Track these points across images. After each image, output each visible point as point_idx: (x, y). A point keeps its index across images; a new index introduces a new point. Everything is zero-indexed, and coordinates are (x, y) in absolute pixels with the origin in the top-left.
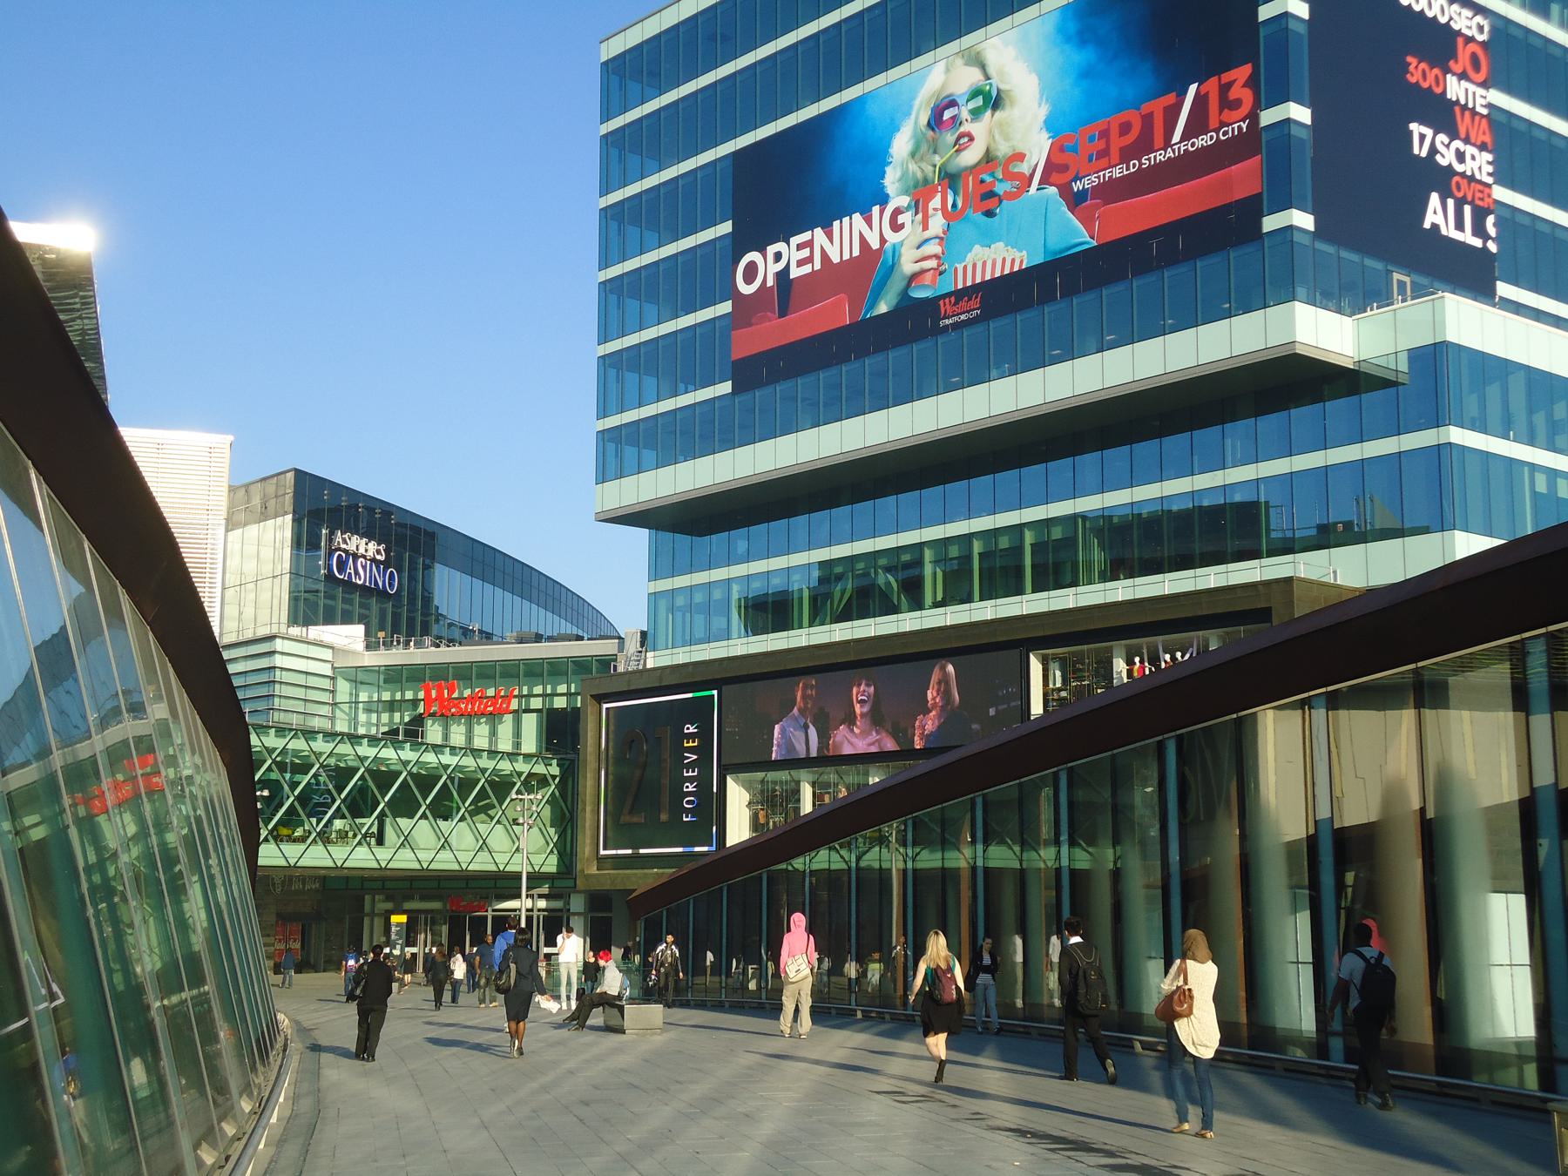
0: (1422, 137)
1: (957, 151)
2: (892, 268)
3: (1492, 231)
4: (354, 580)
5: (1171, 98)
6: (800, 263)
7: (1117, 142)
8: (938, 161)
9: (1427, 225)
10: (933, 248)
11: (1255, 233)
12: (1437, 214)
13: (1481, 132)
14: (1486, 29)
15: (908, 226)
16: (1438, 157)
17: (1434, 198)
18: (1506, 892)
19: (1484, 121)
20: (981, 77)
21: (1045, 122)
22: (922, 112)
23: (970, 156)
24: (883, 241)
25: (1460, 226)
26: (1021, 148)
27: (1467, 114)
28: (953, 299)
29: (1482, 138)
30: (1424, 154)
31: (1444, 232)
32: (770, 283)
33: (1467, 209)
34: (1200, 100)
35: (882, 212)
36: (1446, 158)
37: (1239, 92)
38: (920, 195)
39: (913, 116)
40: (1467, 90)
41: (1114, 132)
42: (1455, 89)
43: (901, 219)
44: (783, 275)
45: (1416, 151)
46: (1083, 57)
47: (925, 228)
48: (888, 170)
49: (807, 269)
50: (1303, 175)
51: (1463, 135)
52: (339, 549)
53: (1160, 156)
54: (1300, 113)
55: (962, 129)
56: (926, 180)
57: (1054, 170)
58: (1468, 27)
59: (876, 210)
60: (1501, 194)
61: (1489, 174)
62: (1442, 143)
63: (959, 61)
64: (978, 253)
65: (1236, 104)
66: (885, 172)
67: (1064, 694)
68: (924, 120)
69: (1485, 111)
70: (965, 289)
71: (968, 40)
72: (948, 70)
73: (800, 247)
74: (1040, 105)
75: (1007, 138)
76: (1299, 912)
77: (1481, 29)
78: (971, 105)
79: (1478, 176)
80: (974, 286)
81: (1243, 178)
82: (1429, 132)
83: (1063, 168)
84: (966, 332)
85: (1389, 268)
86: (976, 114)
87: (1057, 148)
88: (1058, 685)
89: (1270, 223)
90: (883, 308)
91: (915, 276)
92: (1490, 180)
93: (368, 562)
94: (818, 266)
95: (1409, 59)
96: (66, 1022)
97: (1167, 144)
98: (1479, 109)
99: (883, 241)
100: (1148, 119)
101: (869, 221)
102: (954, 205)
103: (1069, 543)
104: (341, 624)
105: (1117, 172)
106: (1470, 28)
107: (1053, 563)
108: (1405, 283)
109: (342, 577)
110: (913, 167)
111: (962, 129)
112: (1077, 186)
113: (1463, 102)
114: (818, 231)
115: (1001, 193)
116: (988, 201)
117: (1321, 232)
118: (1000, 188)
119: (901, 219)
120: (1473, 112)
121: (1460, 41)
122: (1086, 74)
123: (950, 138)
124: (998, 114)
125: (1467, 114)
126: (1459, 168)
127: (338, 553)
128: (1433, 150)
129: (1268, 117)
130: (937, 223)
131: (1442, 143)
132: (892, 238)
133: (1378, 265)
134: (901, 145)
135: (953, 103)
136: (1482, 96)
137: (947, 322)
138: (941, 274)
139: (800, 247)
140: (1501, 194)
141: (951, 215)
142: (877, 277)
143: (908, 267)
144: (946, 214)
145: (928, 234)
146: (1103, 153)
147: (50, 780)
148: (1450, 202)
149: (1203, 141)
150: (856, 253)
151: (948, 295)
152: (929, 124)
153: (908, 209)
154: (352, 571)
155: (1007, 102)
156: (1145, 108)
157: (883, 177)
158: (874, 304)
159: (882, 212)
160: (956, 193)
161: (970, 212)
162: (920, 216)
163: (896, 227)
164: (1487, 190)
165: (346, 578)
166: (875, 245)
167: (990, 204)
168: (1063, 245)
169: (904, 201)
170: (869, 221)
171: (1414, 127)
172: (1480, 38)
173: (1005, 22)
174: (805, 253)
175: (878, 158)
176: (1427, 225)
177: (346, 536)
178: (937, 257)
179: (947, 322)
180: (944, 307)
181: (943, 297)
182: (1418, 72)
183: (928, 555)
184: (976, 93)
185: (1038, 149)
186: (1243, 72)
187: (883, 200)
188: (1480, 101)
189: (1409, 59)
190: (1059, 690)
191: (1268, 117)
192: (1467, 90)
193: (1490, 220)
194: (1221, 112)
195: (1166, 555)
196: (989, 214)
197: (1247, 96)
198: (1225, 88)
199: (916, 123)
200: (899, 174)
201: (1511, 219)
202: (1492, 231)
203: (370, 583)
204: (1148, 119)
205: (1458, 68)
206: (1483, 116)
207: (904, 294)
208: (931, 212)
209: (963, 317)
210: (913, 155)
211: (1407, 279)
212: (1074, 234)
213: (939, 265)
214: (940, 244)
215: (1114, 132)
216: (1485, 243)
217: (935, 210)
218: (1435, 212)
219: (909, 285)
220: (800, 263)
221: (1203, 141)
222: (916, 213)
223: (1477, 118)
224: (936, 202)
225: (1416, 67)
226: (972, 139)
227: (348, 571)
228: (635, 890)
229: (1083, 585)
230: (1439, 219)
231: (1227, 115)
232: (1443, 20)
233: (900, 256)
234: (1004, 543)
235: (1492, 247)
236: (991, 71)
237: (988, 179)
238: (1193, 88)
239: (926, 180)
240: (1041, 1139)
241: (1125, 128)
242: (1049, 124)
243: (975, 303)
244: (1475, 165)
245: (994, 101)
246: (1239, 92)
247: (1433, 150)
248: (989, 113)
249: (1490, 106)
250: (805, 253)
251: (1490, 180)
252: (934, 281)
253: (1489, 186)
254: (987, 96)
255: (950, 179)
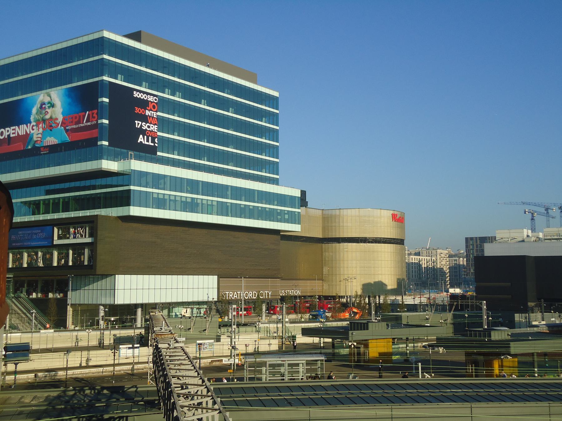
0: (138, 124)
1: (45, 115)
2: (32, 138)
3: (156, 142)
5: (83, 113)
6: (13, 133)
7: (75, 120)
8: (41, 116)
9: (139, 142)
10: (40, 136)
11: (96, 145)
12: (141, 139)
13: (155, 121)
14: (157, 100)
15: (35, 130)
16: (143, 127)
17: (141, 136)
18: (125, 275)
19: (156, 119)
20: (50, 99)
21: (62, 112)
22: (39, 105)
23: (48, 117)
24: (30, 132)
25: (148, 141)
26: (57, 117)
27: (151, 118)
28: (43, 148)
29: (155, 122)
30: (139, 127)
31: (143, 143)
32: (6, 137)
33: (150, 138)
34: (89, 115)
35: (30, 125)
36: (145, 127)
37: (95, 115)
38: (38, 122)
39: (37, 105)
40: (151, 113)
41: (74, 118)
42: (148, 113)
43: (34, 128)
44: (9, 136)
45: (137, 127)
46: (69, 100)
47: (39, 131)
48: (32, 116)
49: (14, 135)
50: (106, 133)
51: (150, 122)
53: (82, 125)
54: (106, 122)
55: (46, 110)
56: (39, 120)
57: (63, 124)
58: (152, 100)
59: (29, 124)
60: (159, 134)
61: (156, 130)
62: (144, 124)
63: (46, 95)
64: (48, 139)
65: (94, 118)
66: (31, 116)
67: (61, 235)
68: (39, 106)
69: (156, 117)
70: (46, 146)
71: (48, 90)
72: (44, 96)
73: (13, 130)
74: (61, 109)
75: (55, 115)
76: (104, 279)
77: (156, 100)
78: (48, 105)
79: (153, 130)
80: (48, 146)
81: (94, 133)
82: (140, 123)
83: (65, 124)
84: (46, 156)
85: (128, 151)
86: (49, 107)
87: (64, 119)
88: (61, 234)
89: (99, 143)
90: (30, 147)
91: (37, 141)
92: (157, 131)
94: (16, 135)
95: (136, 108)
97: (83, 123)
98: (154, 116)
99: (30, 132)
100: (80, 116)
101: (27, 127)
102: (44, 127)
103: (68, 202)
105: (74, 127)
106: (153, 100)
107: (129, 191)
108: (132, 154)
110: (36, 116)
111: (46, 110)
112: (67, 128)
113: (150, 115)
114: (17, 127)
115: (53, 126)
116: (51, 127)
117: (110, 145)
118: (53, 125)
119: (34, 128)
120: (153, 117)
121: (150, 103)
122: (69, 104)
123: (44, 112)
124: (53, 108)
125: (151, 118)
126: (149, 129)
128: (141, 126)
129: (100, 121)
130: (41, 130)
131: (144, 124)
132: (32, 132)
133: (125, 151)
134: (34, 111)
135: (44, 104)
136: (155, 114)
137: (42, 153)
138: (41, 142)
139: (13, 130)
140: (159, 134)
141: (44, 129)
142: (28, 140)
143: (35, 139)
144: (43, 129)
145: (39, 132)
146: (72, 122)
147: (293, 341)
148: (145, 137)
149: (89, 124)
150: (25, 134)
151: (43, 147)
152: (40, 107)
153: (35, 126)
155: (55, 106)
156: (80, 114)
157: (30, 117)
158: (28, 146)
159: (30, 125)
160: (45, 124)
161: (47, 129)
162: (37, 128)
163: (33, 129)
164: (155, 133)
166: (29, 133)
167: (51, 128)
168: (64, 140)
169: (34, 124)
170: (27, 127)
171: (136, 122)
172: (156, 102)
173: (55, 88)
174: (14, 131)
175: (30, 113)
176: (139, 142)
178: (40, 138)
179: (42, 153)
180: (42, 149)
181: (41, 147)
182: (137, 110)
183: (41, 202)
184: (49, 103)
185: (60, 119)
186: (95, 111)
187: (30, 123)
188: (154, 115)
189: (136, 108)
190: (61, 234)
191: (100, 121)
193: (156, 139)
194: (92, 119)
196: (51, 130)
197: (96, 116)
198: (93, 114)
199: (37, 107)
200: (33, 117)
201: (162, 139)
202: (156, 142)
204: (80, 116)
205: (149, 109)
206: (155, 118)
207: (34, 145)
208: (40, 127)
209: (45, 152)
210: (37, 113)
211: (133, 153)
212: (67, 138)
213: (41, 140)
214: (41, 135)
215: (74, 118)
216: (154, 144)
217: (41, 127)
218: (141, 139)
219: (35, 143)
220: (13, 133)
221: (89, 124)
222: (37, 127)
223: (154, 118)
224: (41, 126)
225: (137, 110)
226: (48, 113)
229: (71, 211)
230: (142, 140)
231: (93, 119)
232: (146, 99)
233: (33, 136)
234: (56, 201)
235: (156, 145)
236: (52, 99)
237: (51, 123)
238: (88, 112)
239: (39, 120)
241: (76, 118)
242: (62, 113)
243: (48, 149)
244: (153, 128)
245: (53, 106)
246: (95, 115)
247: (141, 126)
248: (51, 108)
249: (157, 116)
250: (14, 131)
251: (157, 131)
252: (40, 143)
253: (157, 132)
254: (51, 104)
255: (44, 121)
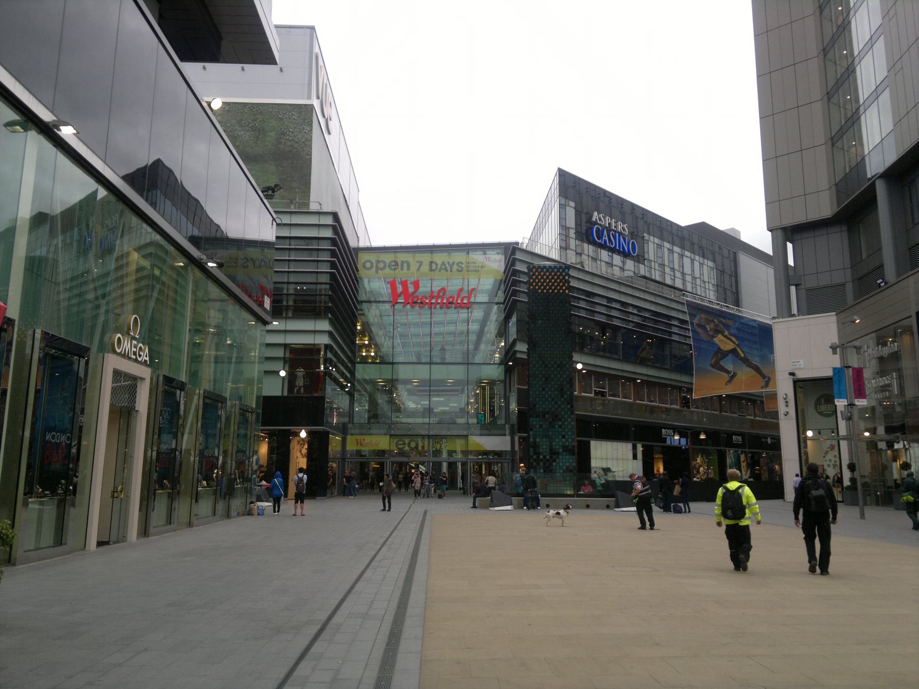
4: (608, 244)
40: (910, 317)
52: (598, 224)
93: (617, 235)
96: (258, 335)
102: (423, 447)
104: (781, 451)
109: (600, 241)
127: (596, 226)
154: (607, 238)
165: (603, 242)
177: (601, 215)
192: (910, 317)
195: (233, 366)
203: (619, 247)
227: (604, 238)
228: (147, 165)
240: (512, 262)
